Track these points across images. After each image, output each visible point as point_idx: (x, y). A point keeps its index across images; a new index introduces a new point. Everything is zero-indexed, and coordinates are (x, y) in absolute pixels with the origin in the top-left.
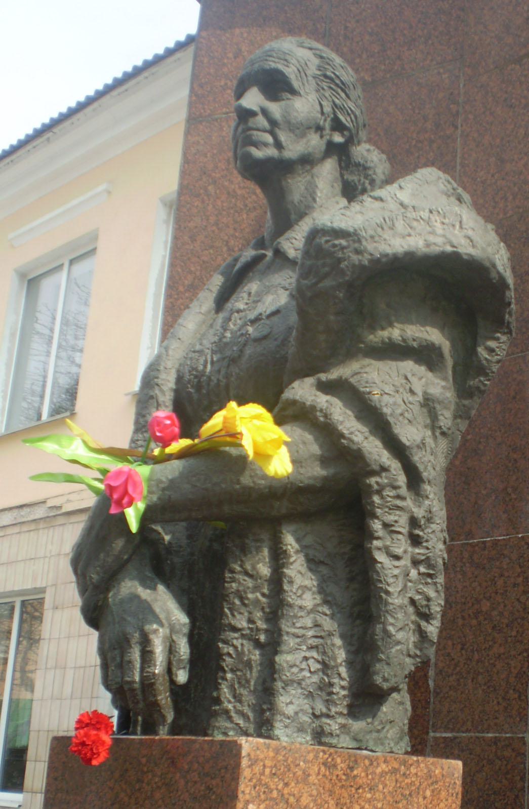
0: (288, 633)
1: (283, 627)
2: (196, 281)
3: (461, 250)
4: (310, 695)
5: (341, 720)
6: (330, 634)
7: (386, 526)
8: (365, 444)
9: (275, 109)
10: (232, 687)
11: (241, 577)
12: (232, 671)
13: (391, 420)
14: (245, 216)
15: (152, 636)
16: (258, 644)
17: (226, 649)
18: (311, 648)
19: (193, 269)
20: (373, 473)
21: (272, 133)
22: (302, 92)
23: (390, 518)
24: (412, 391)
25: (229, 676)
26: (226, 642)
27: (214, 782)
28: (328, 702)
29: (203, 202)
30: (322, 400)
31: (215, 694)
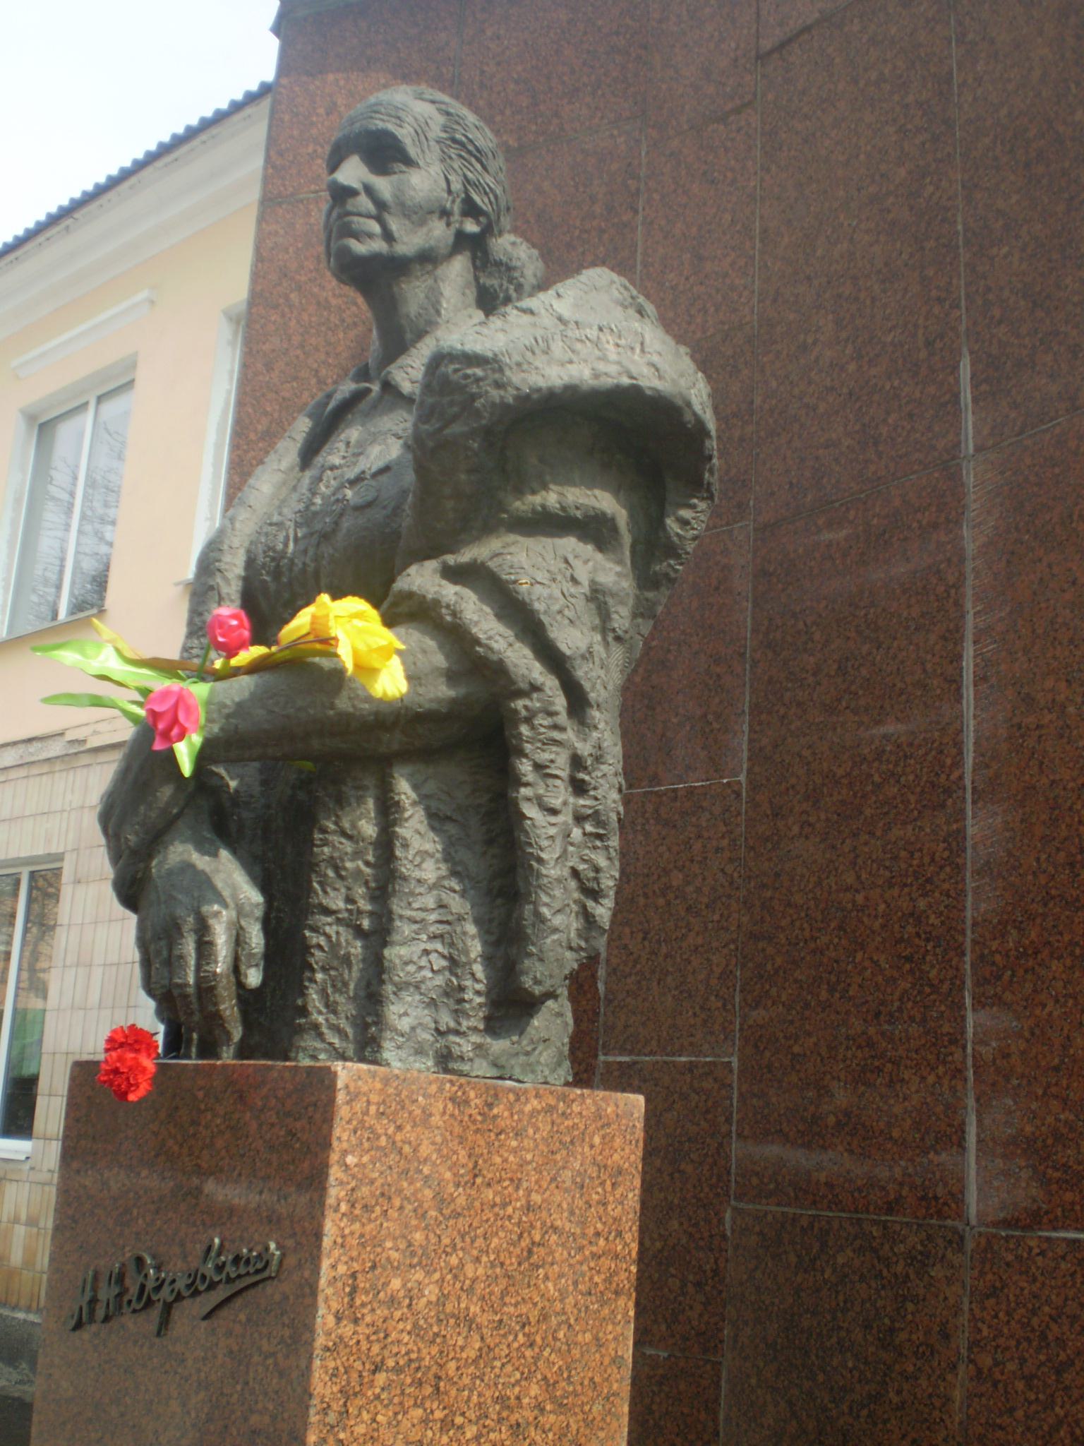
0: (401, 917)
3: (643, 383)
4: (432, 1003)
5: (475, 1038)
8: (509, 653)
9: (383, 185)
11: (336, 839)
13: (545, 619)
14: (341, 335)
15: (211, 922)
16: (359, 932)
17: (315, 939)
18: (433, 937)
20: (520, 694)
22: (421, 163)
25: (319, 976)
26: (315, 929)
28: (457, 1013)
29: (283, 316)
31: (300, 1002)
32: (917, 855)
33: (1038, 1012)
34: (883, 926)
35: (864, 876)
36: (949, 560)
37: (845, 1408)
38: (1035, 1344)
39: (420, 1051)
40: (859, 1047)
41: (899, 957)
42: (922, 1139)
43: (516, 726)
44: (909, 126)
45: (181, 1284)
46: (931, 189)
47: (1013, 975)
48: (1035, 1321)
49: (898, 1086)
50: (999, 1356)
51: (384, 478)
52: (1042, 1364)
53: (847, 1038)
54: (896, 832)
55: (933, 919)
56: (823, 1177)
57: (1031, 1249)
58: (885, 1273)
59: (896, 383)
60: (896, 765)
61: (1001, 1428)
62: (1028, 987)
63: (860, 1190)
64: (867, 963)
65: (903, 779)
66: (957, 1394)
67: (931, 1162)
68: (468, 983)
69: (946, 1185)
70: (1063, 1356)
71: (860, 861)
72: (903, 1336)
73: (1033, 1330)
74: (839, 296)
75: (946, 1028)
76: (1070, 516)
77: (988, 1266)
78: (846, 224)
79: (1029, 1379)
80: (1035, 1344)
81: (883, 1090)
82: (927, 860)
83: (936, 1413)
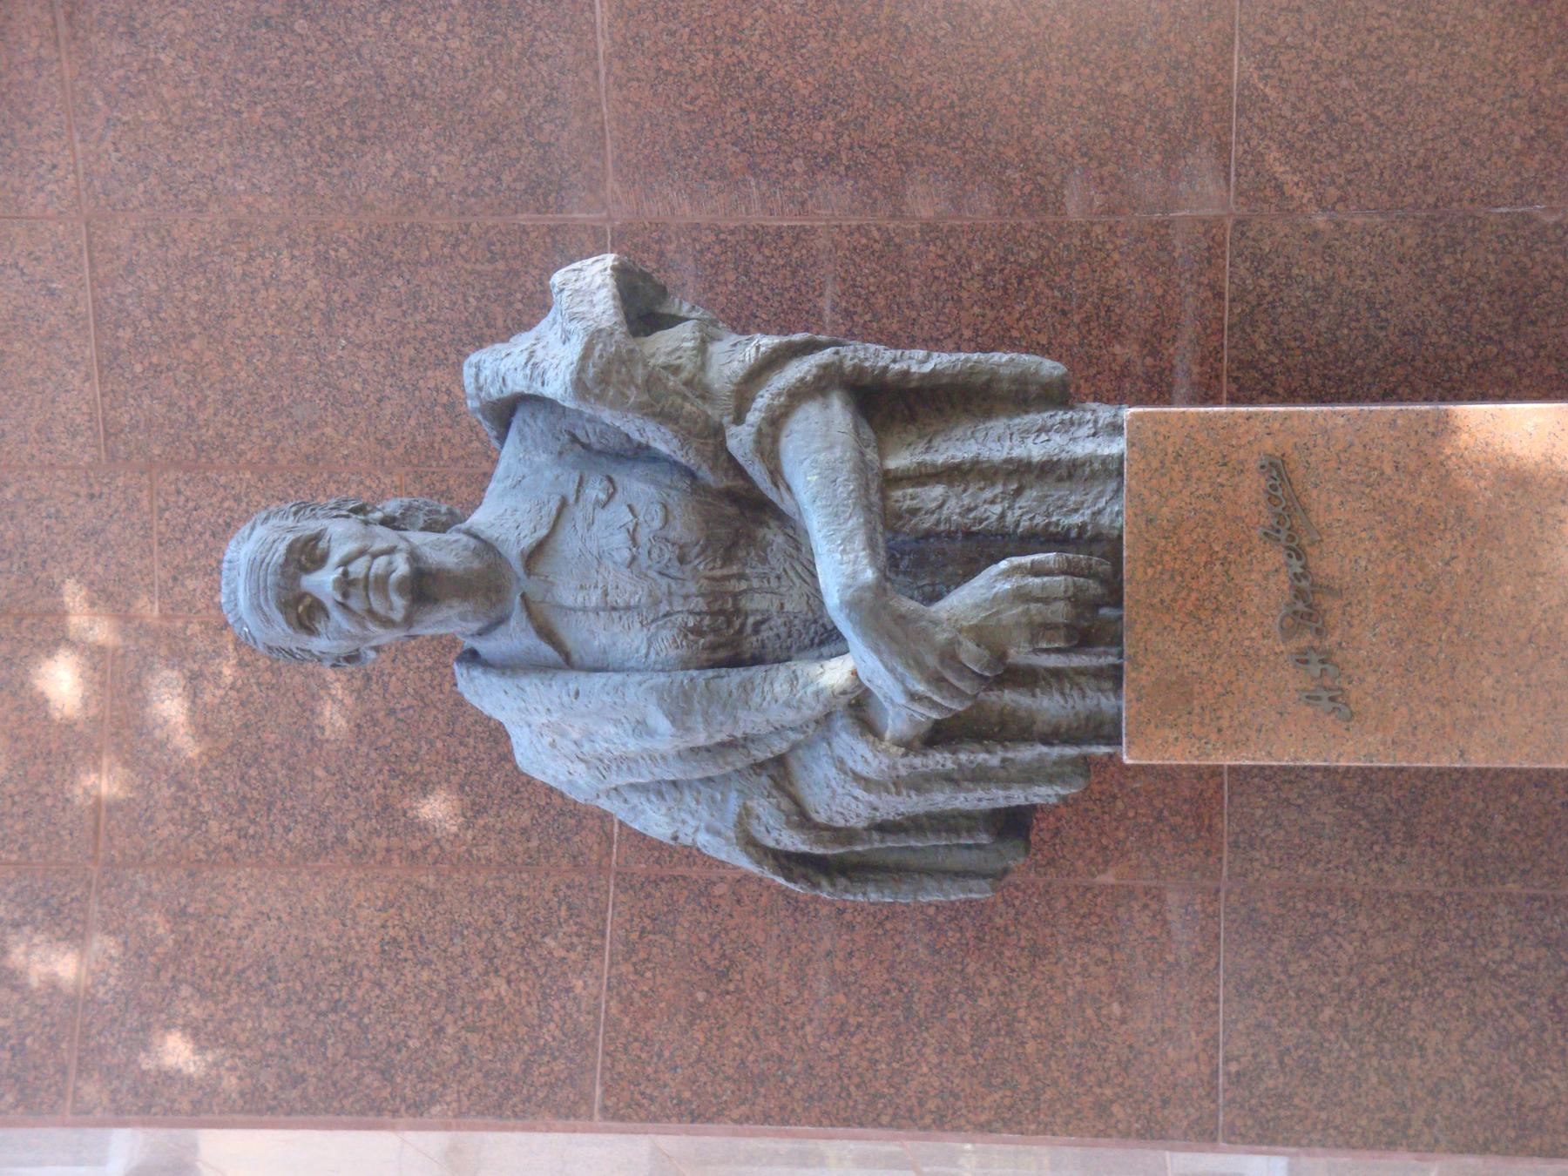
2: (377, 1064)
6: (1008, 427)
10: (1066, 515)
11: (945, 512)
12: (1049, 515)
17: (1025, 524)
19: (355, 1073)
21: (375, 556)
26: (1017, 525)
27: (1170, 450)
30: (754, 417)
32: (937, 273)
33: (1069, 149)
34: (992, 307)
35: (949, 330)
36: (694, 240)
37: (1381, 334)
38: (1314, 144)
40: (1089, 331)
41: (1018, 290)
42: (1163, 264)
44: (268, 273)
46: (343, 250)
47: (1042, 175)
48: (1299, 145)
49: (1121, 290)
50: (1327, 180)
52: (1330, 137)
53: (1081, 345)
54: (916, 297)
55: (990, 256)
56: (1196, 369)
57: (1245, 152)
58: (1270, 298)
59: (519, 296)
60: (859, 296)
61: (1381, 174)
62: (1051, 158)
63: (1205, 329)
64: (1022, 324)
65: (872, 289)
66: (1359, 221)
67: (1181, 256)
69: (1198, 240)
70: (1323, 117)
71: (935, 334)
72: (1318, 277)
73: (1305, 147)
74: (412, 360)
75: (1076, 241)
76: (689, 112)
77: (1260, 194)
78: (340, 353)
79: (1343, 149)
80: (1314, 144)
81: (1125, 305)
82: (941, 263)
83: (1377, 240)
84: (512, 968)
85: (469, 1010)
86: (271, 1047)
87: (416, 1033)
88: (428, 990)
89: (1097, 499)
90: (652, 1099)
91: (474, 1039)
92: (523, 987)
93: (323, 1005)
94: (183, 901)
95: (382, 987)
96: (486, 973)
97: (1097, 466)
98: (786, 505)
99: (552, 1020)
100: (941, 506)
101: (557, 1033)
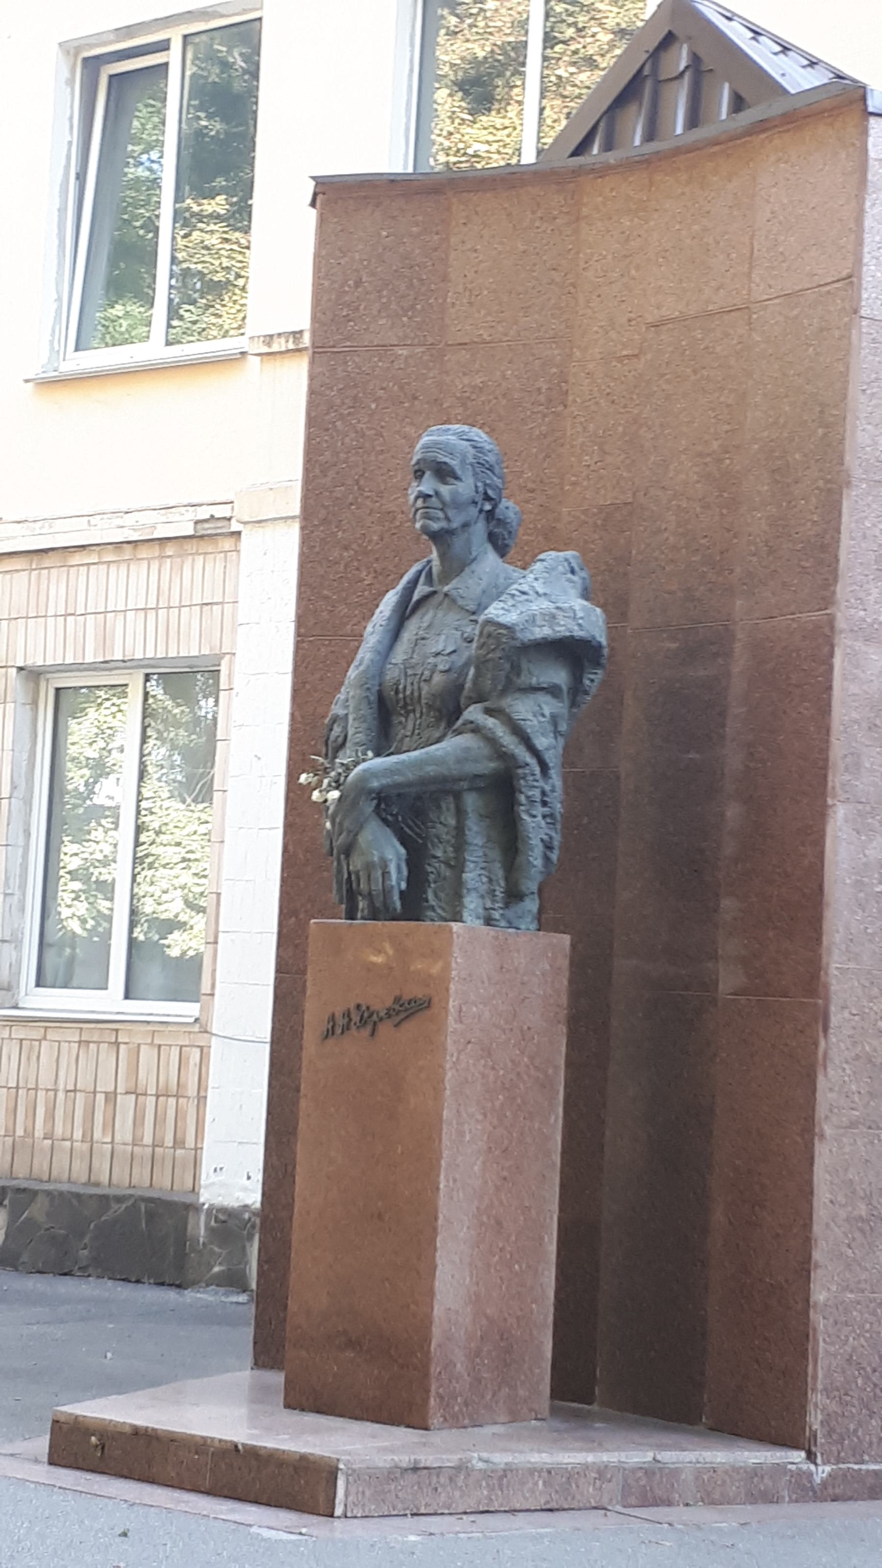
0: (469, 861)
1: (467, 857)
3: (575, 634)
4: (482, 897)
5: (501, 912)
7: (528, 797)
8: (516, 751)
9: (445, 490)
11: (439, 825)
13: (531, 736)
14: (373, 458)
15: (388, 863)
16: (449, 865)
17: (430, 869)
18: (482, 868)
20: (520, 767)
22: (464, 479)
23: (530, 793)
24: (543, 715)
25: (433, 885)
26: (429, 865)
28: (493, 901)
29: (332, 438)
31: (424, 896)
39: (478, 918)
43: (518, 780)
45: (382, 1014)
51: (454, 657)
68: (497, 888)
84: (377, 586)
85: (355, 564)
86: (342, 456)
87: (345, 536)
88: (367, 540)
89: (443, 909)
90: (306, 668)
91: (342, 568)
92: (366, 593)
93: (362, 482)
94: (421, 398)
95: (370, 514)
96: (375, 572)
97: (458, 909)
98: (450, 735)
99: (349, 610)
100: (441, 823)
101: (342, 613)
